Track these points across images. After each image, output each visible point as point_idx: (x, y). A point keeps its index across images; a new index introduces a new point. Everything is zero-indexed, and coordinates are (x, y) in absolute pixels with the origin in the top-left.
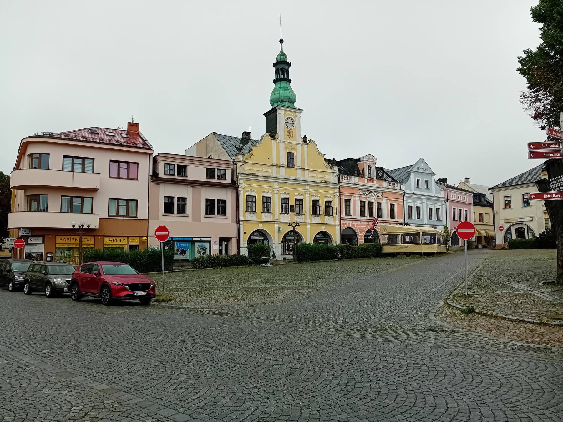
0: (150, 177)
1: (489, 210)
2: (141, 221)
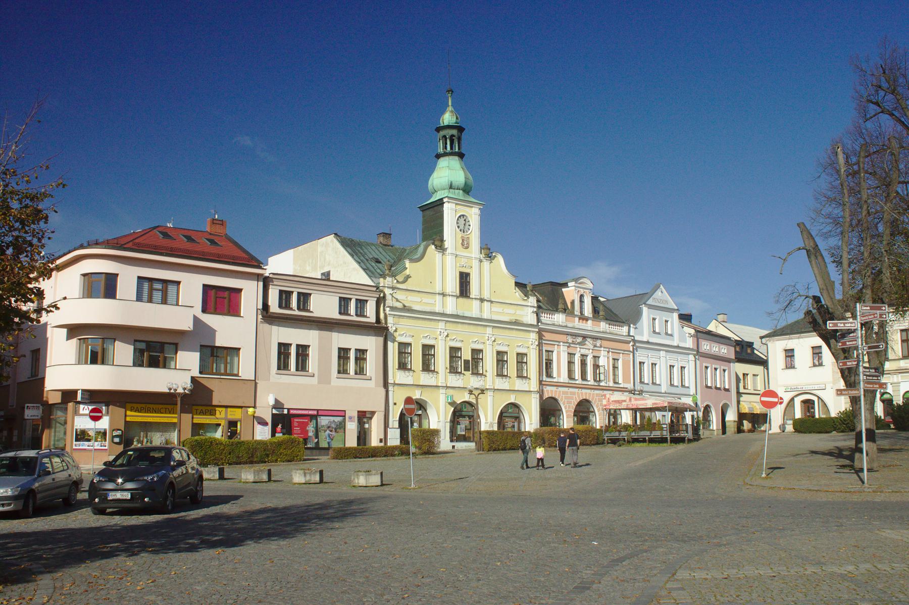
0: (259, 312)
1: (759, 369)
2: (246, 381)
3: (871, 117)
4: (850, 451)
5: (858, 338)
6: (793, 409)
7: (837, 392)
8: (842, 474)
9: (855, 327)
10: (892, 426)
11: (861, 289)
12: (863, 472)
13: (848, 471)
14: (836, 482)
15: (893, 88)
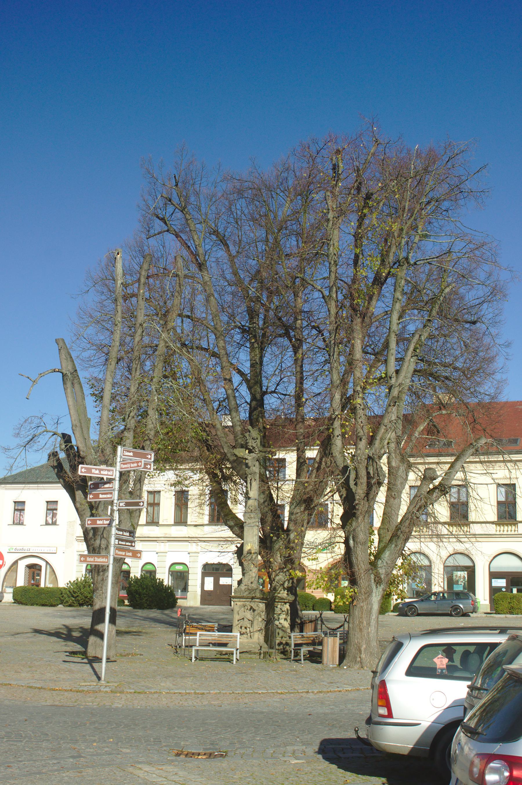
3: (155, 235)
4: (81, 632)
5: (114, 490)
6: (15, 574)
7: (81, 558)
8: (72, 665)
9: (112, 475)
10: (126, 602)
11: (122, 432)
12: (101, 662)
13: (79, 660)
14: (64, 676)
15: (183, 205)
